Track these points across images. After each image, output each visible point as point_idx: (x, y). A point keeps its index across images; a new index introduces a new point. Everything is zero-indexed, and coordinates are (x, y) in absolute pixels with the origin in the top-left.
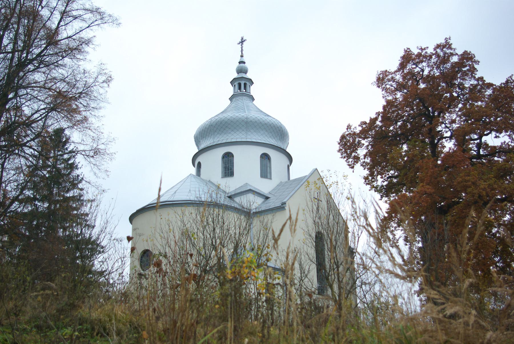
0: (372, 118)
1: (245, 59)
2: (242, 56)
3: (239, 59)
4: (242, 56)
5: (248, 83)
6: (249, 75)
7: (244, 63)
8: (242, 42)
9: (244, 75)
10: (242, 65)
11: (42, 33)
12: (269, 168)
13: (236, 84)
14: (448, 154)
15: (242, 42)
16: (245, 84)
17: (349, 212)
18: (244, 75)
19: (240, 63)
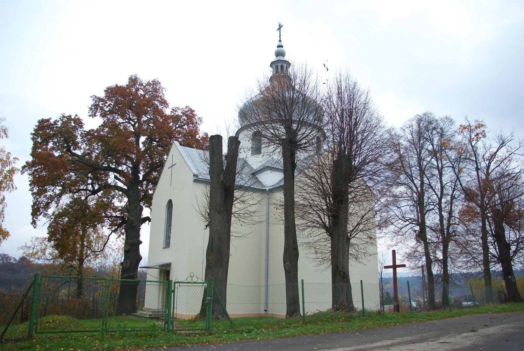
0: (141, 246)
1: (283, 43)
2: (280, 41)
3: (277, 43)
4: (280, 41)
5: (285, 65)
6: (286, 58)
7: (282, 47)
8: (280, 27)
9: (281, 58)
10: (280, 48)
11: (77, 187)
12: (388, 342)
13: (274, 66)
14: (142, 209)
15: (280, 27)
16: (282, 67)
17: (327, 91)
18: (281, 58)
19: (278, 47)
